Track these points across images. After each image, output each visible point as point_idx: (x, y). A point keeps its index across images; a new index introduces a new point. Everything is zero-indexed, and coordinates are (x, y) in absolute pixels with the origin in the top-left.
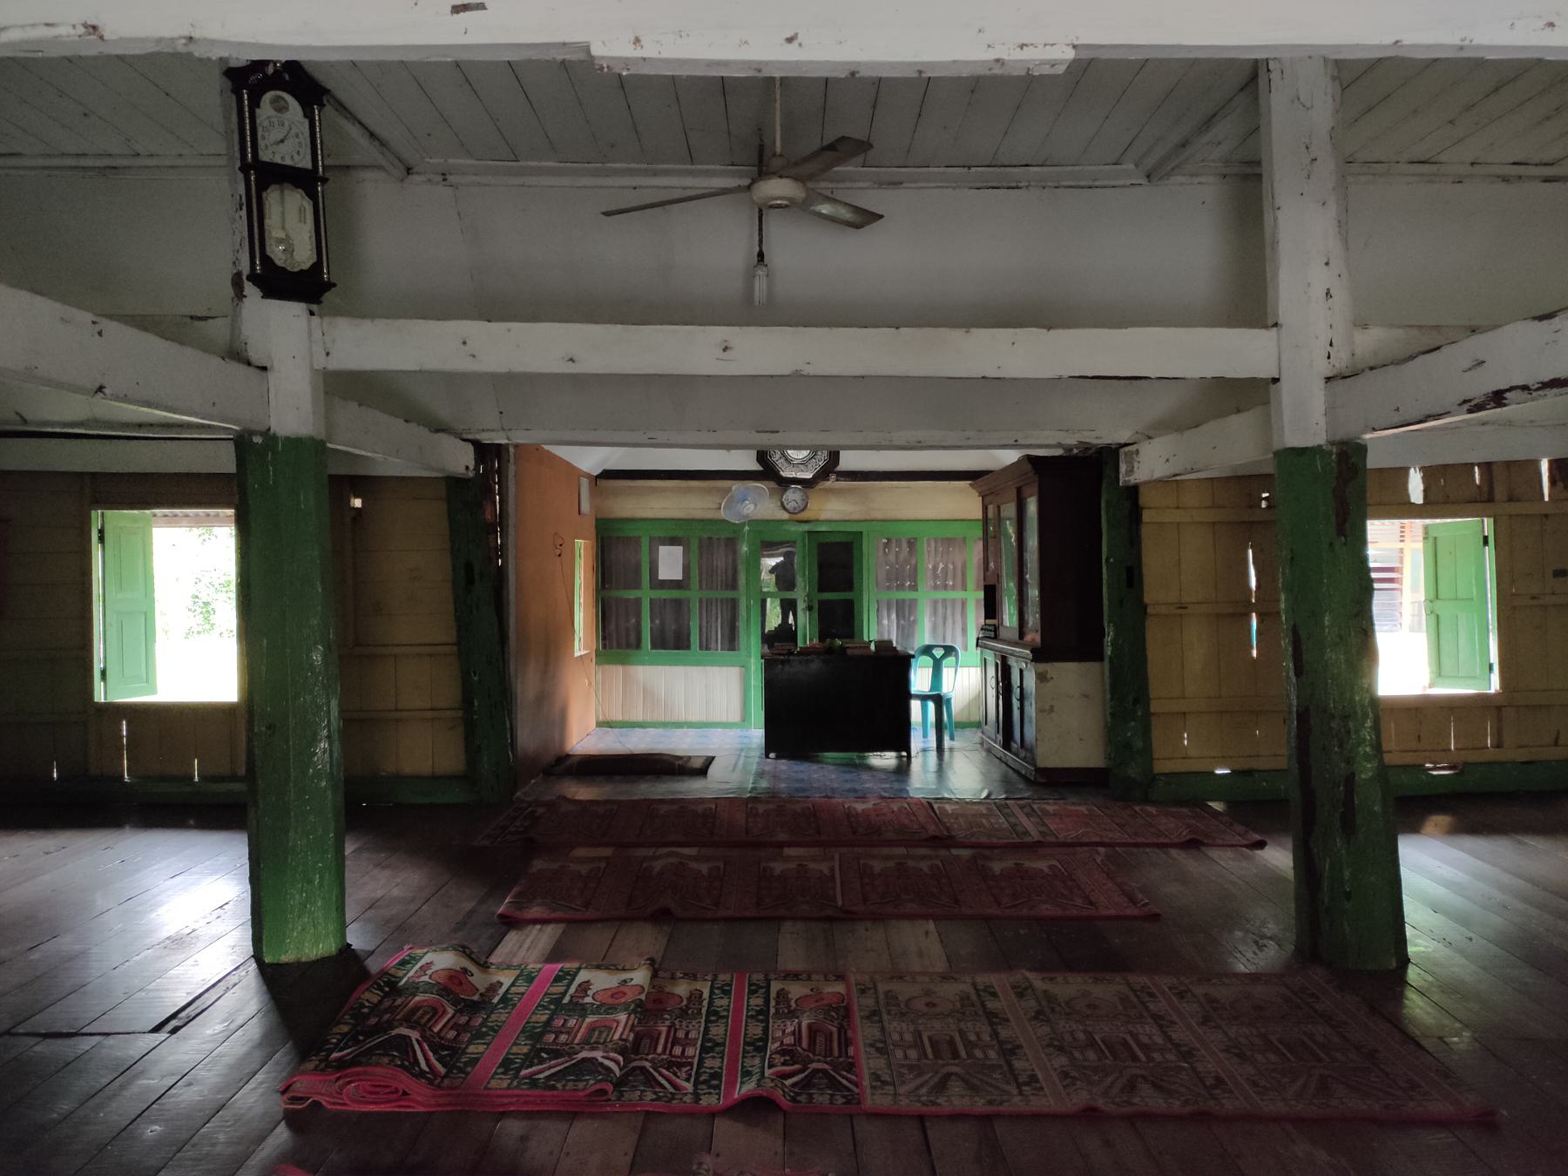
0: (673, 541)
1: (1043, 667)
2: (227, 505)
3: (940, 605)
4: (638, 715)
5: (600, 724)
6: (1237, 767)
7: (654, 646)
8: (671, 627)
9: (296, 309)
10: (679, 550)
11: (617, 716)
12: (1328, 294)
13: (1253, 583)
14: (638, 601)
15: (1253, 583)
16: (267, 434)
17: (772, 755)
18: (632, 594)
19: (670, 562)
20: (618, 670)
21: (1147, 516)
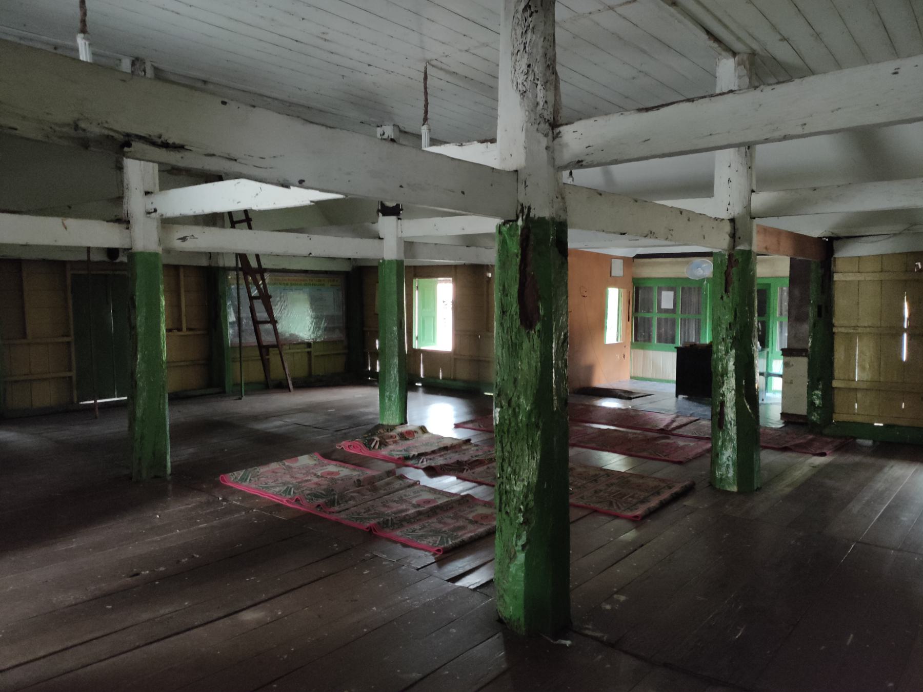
0: (669, 289)
1: (788, 359)
2: (450, 276)
3: (669, 323)
4: (649, 375)
5: (631, 378)
6: (889, 422)
7: (659, 340)
8: (670, 332)
9: (393, 219)
10: (672, 293)
11: (640, 375)
12: (729, 181)
13: (906, 314)
14: (649, 320)
15: (906, 314)
16: (383, 259)
17: (681, 397)
18: (648, 315)
19: (667, 300)
20: (640, 352)
21: (836, 277)
